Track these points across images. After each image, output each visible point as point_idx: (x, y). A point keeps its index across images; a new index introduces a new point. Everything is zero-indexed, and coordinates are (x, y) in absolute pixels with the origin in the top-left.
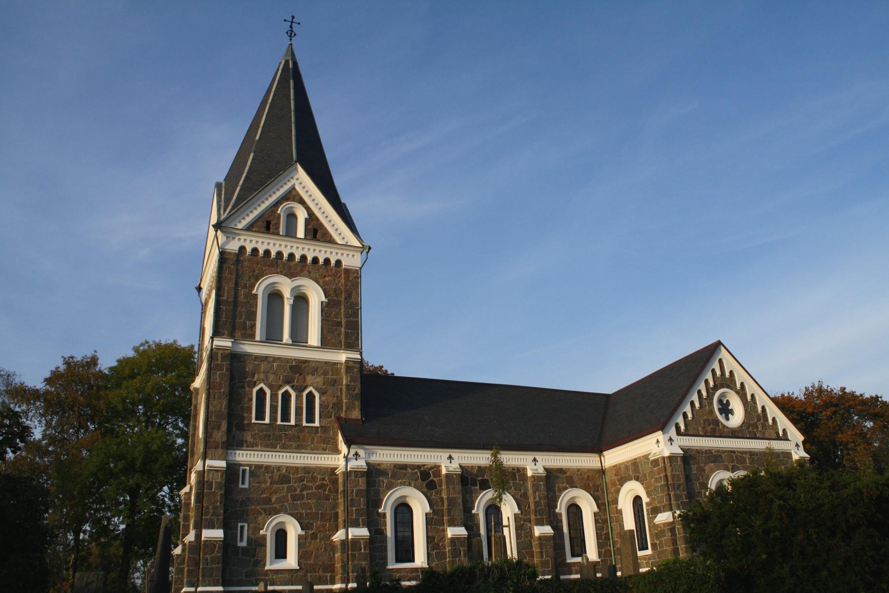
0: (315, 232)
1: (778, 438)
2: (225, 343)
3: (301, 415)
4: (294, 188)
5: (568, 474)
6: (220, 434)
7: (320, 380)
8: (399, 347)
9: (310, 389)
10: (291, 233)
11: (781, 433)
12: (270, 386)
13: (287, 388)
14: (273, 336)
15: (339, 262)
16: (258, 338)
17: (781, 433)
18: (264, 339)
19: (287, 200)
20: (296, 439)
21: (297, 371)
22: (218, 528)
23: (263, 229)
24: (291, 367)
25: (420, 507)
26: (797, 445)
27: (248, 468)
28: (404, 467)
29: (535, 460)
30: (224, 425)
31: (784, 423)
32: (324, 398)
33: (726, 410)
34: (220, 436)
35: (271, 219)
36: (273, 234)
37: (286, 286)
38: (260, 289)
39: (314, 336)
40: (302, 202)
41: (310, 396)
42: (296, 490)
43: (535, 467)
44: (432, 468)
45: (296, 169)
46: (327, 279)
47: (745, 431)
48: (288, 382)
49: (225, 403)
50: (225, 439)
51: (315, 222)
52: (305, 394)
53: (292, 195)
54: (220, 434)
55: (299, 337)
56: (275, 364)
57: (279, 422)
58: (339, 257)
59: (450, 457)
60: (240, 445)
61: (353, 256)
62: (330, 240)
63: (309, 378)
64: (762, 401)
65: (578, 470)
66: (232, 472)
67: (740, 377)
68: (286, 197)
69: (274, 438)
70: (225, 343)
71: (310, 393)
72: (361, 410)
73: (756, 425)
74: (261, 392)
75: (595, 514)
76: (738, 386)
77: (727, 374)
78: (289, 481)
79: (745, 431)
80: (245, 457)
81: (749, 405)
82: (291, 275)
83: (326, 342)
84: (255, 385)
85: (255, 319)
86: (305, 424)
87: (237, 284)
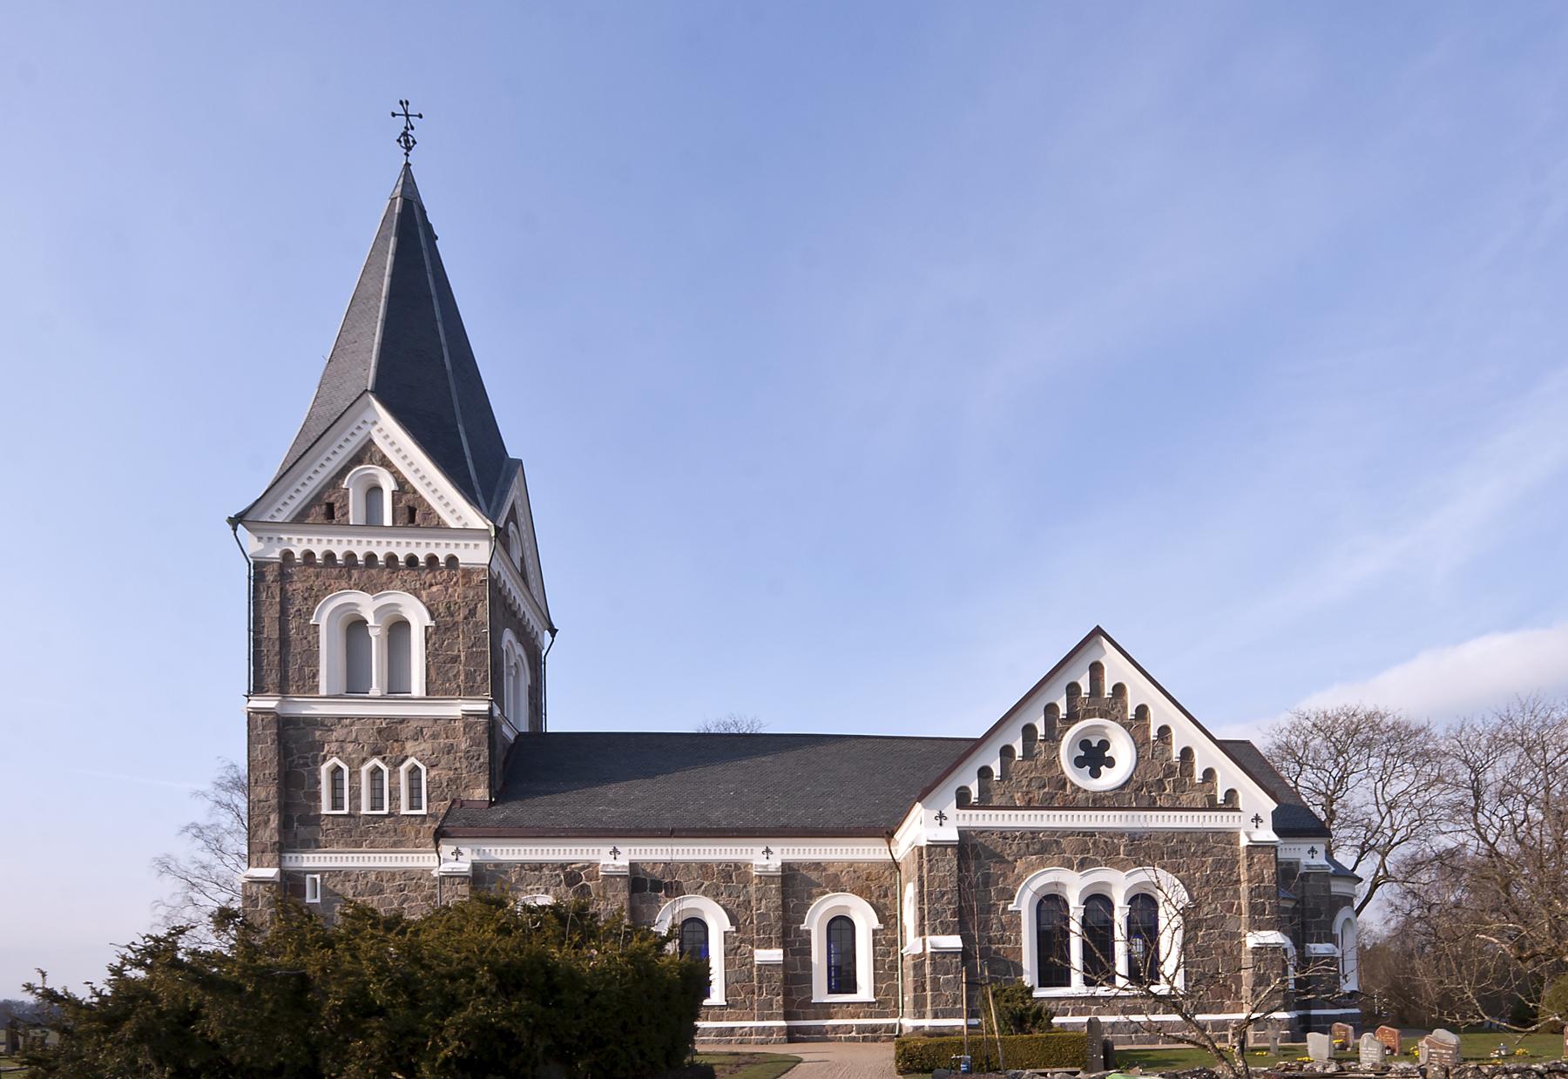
0: (412, 511)
1: (1212, 806)
2: (269, 703)
3: (359, 797)
4: (371, 441)
5: (831, 871)
6: (268, 832)
7: (426, 746)
8: (583, 697)
9: (412, 761)
10: (372, 521)
11: (1220, 797)
12: (348, 762)
13: (376, 761)
14: (355, 685)
15: (452, 560)
16: (323, 691)
17: (1220, 797)
18: (341, 689)
19: (361, 463)
20: (392, 831)
21: (388, 736)
22: (952, 933)
23: (321, 519)
24: (380, 731)
25: (718, 923)
26: (1257, 818)
27: (318, 877)
28: (538, 867)
29: (768, 851)
30: (274, 820)
31: (1230, 775)
32: (433, 773)
33: (1094, 757)
34: (270, 834)
35: (332, 499)
36: (339, 524)
37: (367, 605)
38: (325, 616)
39: (417, 686)
40: (385, 463)
41: (414, 771)
42: (391, 903)
43: (766, 862)
44: (584, 868)
45: (369, 405)
46: (434, 589)
47: (1133, 795)
48: (376, 753)
49: (273, 790)
50: (276, 838)
51: (410, 496)
52: (403, 768)
53: (366, 453)
54: (268, 832)
55: (396, 686)
56: (354, 728)
57: (365, 810)
58: (452, 551)
59: (615, 851)
60: (311, 844)
61: (467, 545)
62: (439, 527)
63: (410, 746)
64: (1183, 735)
65: (851, 864)
66: (291, 883)
67: (1139, 692)
68: (357, 459)
69: (355, 832)
70: (269, 703)
71: (415, 769)
72: (490, 787)
73: (1165, 777)
74: (337, 770)
75: (875, 932)
76: (1131, 711)
77: (1108, 690)
78: (381, 891)
79: (1133, 795)
80: (310, 861)
81: (1152, 743)
82: (371, 587)
83: (433, 690)
84: (324, 759)
85: (317, 665)
86: (404, 811)
87: (283, 611)
